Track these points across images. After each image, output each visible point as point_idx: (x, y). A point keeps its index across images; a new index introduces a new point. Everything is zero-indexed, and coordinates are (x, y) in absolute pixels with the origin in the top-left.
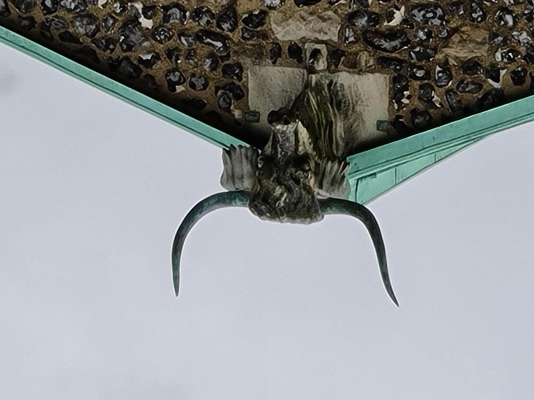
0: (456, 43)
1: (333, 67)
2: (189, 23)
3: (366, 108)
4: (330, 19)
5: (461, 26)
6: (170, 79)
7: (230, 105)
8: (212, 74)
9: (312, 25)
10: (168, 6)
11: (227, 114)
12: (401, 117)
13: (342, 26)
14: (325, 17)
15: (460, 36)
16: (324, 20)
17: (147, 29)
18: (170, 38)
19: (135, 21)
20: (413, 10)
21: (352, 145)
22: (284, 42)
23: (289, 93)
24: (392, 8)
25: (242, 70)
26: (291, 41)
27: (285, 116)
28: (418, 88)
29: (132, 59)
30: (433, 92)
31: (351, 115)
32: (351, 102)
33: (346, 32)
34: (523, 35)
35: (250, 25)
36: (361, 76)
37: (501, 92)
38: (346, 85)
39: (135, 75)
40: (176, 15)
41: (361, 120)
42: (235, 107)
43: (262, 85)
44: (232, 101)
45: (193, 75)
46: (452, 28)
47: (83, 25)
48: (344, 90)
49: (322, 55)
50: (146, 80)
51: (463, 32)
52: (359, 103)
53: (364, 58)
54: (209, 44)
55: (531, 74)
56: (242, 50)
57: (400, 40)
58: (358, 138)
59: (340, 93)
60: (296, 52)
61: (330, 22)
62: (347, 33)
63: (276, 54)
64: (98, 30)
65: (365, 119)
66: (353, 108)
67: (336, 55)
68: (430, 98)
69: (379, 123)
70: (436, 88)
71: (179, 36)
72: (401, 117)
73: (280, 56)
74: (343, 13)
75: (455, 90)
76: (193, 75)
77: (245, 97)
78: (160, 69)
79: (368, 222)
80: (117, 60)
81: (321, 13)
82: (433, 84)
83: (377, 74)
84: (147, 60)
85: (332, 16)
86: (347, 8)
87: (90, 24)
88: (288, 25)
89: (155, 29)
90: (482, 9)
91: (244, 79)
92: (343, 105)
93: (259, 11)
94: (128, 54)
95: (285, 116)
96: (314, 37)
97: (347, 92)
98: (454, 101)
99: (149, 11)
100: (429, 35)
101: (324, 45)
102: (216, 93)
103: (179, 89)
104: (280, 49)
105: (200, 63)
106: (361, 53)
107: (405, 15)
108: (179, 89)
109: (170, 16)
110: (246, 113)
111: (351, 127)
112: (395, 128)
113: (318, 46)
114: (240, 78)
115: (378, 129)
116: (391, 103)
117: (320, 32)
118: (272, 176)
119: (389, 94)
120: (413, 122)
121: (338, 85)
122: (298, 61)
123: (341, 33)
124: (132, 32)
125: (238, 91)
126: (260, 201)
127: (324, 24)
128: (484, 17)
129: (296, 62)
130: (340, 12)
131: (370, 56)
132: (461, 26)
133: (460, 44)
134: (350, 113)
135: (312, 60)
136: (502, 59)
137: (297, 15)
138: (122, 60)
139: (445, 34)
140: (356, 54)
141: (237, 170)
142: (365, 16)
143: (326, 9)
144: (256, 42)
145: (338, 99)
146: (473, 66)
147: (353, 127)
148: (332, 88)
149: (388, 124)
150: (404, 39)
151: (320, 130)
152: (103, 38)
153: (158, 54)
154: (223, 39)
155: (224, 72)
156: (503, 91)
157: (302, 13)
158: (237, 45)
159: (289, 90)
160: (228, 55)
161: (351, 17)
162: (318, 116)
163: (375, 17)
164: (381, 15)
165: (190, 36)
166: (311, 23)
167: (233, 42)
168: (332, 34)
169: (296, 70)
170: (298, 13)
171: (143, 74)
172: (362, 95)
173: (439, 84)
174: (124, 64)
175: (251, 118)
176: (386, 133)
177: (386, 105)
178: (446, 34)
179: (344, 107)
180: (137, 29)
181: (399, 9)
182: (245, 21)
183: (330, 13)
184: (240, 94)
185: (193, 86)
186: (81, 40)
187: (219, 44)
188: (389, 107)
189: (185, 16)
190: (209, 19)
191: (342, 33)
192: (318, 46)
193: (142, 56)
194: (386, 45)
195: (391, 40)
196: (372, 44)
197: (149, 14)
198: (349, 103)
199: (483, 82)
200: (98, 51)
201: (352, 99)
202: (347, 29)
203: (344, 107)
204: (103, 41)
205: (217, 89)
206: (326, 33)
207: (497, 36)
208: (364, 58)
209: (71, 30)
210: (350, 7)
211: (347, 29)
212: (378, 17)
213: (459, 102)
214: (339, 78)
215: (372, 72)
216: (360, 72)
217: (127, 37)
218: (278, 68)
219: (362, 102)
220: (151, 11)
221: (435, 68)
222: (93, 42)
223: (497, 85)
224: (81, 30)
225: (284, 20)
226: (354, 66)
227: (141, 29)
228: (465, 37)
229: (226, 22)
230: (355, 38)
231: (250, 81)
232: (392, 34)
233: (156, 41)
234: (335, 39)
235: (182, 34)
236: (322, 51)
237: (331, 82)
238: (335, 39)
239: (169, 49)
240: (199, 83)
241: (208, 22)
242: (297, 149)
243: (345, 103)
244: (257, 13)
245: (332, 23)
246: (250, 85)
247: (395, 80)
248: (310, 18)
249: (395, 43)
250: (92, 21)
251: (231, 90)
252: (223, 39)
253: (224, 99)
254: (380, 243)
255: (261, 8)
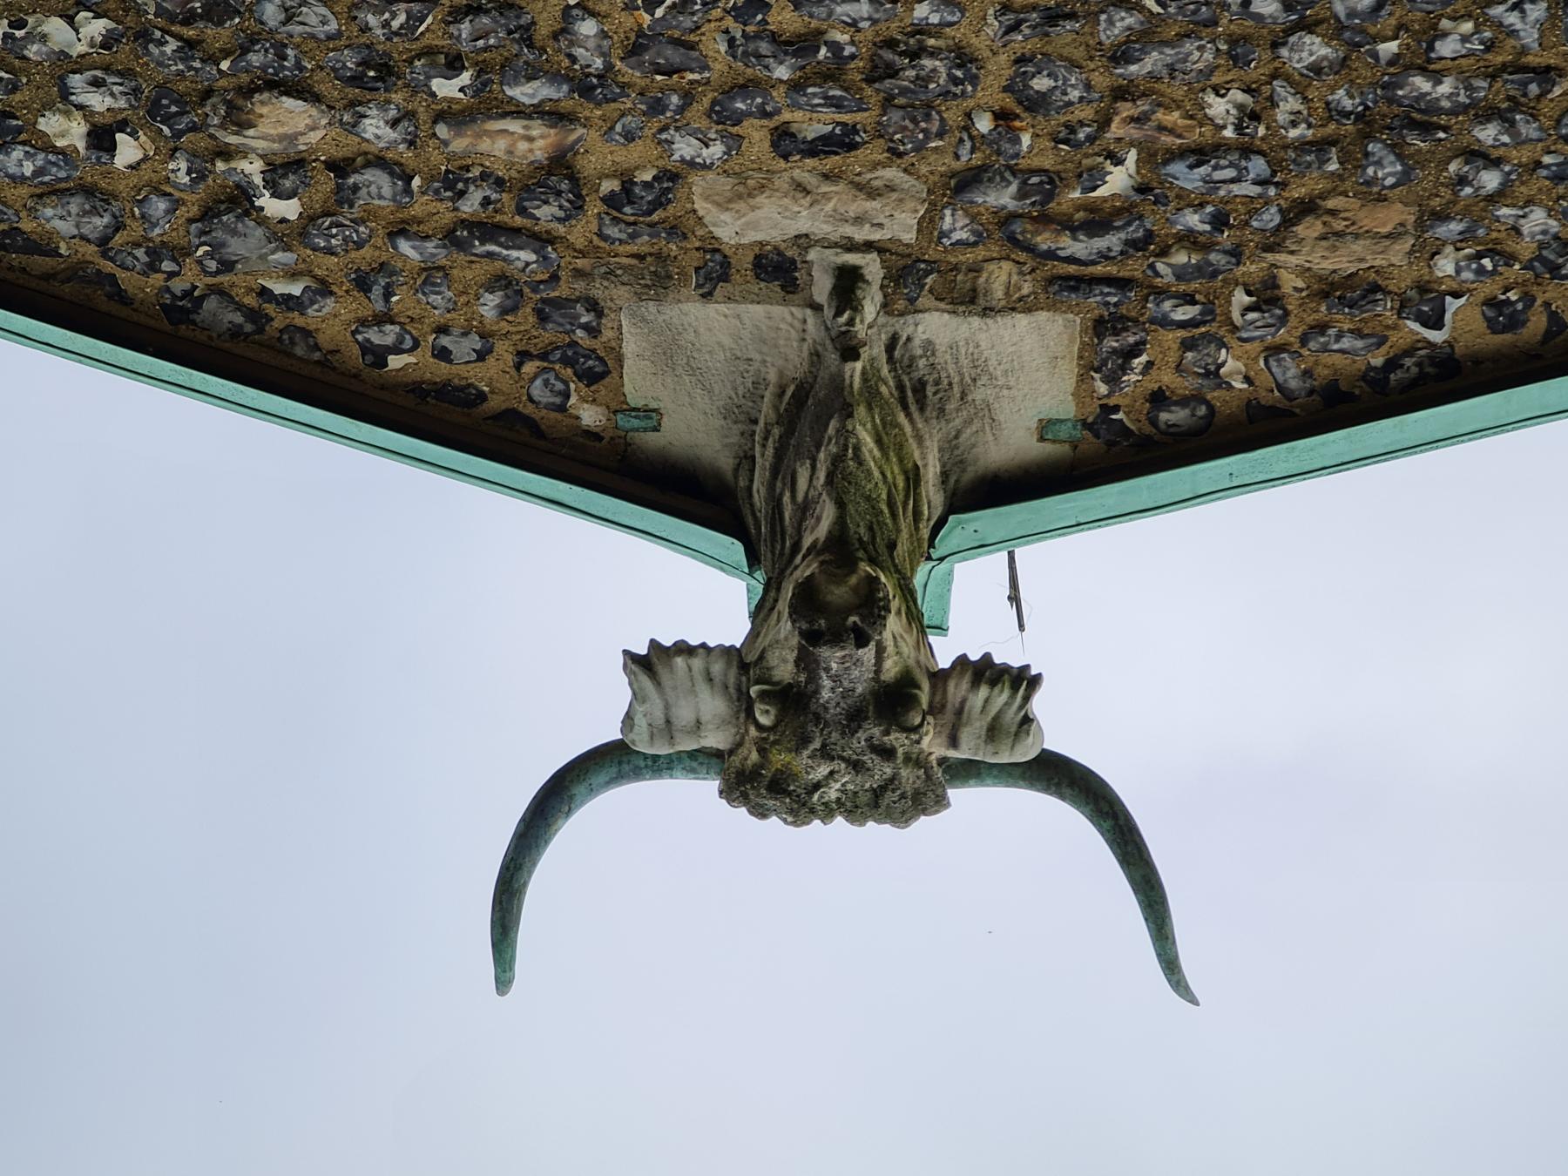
0: (1309, 242)
1: (901, 304)
2: (421, 206)
3: (1005, 392)
4: (890, 188)
5: (1323, 196)
6: (368, 340)
7: (568, 397)
8: (503, 324)
9: (830, 206)
10: (344, 160)
11: (559, 416)
12: (1116, 409)
13: (933, 204)
14: (876, 183)
15: (1324, 223)
16: (873, 194)
17: (283, 221)
18: (359, 245)
19: (240, 199)
20: (1166, 162)
21: (957, 481)
22: (738, 246)
23: (756, 365)
24: (1101, 159)
25: (600, 314)
26: (762, 244)
27: (853, 619)
28: (1175, 346)
29: (238, 292)
30: (1224, 351)
31: (958, 410)
32: (956, 380)
33: (942, 218)
34: (1532, 217)
35: (627, 210)
36: (990, 321)
37: (1448, 350)
38: (941, 342)
39: (249, 328)
40: (380, 188)
41: (987, 420)
42: (583, 400)
43: (669, 353)
44: (572, 386)
45: (442, 330)
46: (1294, 200)
47: (69, 214)
48: (933, 354)
49: (867, 282)
50: (285, 337)
51: (1333, 213)
52: (984, 380)
53: (999, 277)
54: (490, 255)
55: (1547, 305)
56: (604, 269)
57: (1123, 235)
58: (976, 460)
59: (922, 363)
60: (778, 269)
61: (894, 196)
62: (948, 219)
63: (715, 273)
64: (118, 227)
65: (1002, 418)
66: (963, 395)
67: (908, 274)
68: (1212, 368)
69: (1045, 429)
70: (1234, 343)
71: (392, 235)
72: (1116, 409)
73: (725, 277)
74: (932, 173)
75: (1296, 347)
76: (442, 330)
77: (615, 374)
78: (332, 320)
79: (1107, 825)
80: (187, 294)
81: (859, 174)
82: (1222, 332)
83: (1043, 316)
84: (290, 296)
85: (897, 181)
86: (949, 160)
87: (94, 211)
88: (753, 208)
89: (309, 219)
90: (1400, 157)
91: (608, 334)
92: (930, 390)
93: (654, 172)
94: (224, 279)
95: (853, 619)
96: (838, 235)
97: (944, 357)
98: (1290, 374)
99: (285, 176)
100: (1219, 221)
101: (874, 255)
102: (518, 366)
103: (395, 362)
104: (726, 264)
105: (463, 299)
106: (992, 266)
107: (1138, 172)
108: (395, 362)
109: (356, 188)
110: (615, 412)
111: (956, 437)
112: (1097, 436)
113: (852, 259)
114: (593, 331)
115: (1042, 439)
116: (1083, 378)
117: (858, 220)
118: (806, 748)
119: (1080, 357)
120: (1154, 422)
121: (917, 342)
122: (783, 287)
123: (928, 224)
124: (234, 233)
125: (590, 362)
126: (763, 791)
127: (876, 204)
128: (1404, 179)
129: (778, 289)
130: (924, 169)
131: (1021, 273)
132: (1323, 196)
133: (1324, 243)
134: (951, 406)
135: (846, 316)
136: (1458, 272)
137: (782, 182)
138: (203, 298)
139: (1271, 218)
140: (975, 269)
141: (684, 714)
142: (1010, 183)
143: (875, 166)
144: (645, 249)
145: (916, 375)
146: (1363, 297)
147: (964, 436)
148: (897, 354)
149: (1074, 427)
150: (1136, 231)
151: (894, 515)
152: (138, 245)
153: (322, 281)
154: (541, 240)
155: (542, 318)
156: (1452, 347)
157: (797, 173)
158: (583, 254)
159: (757, 357)
160: (555, 278)
161: (965, 182)
162: (883, 474)
163: (1042, 182)
164: (1058, 173)
165: (427, 237)
166: (829, 199)
167: (571, 246)
168: (900, 224)
169: (778, 311)
170: (786, 175)
171: (276, 324)
172: (993, 362)
173: (1245, 335)
174: (211, 304)
175: (636, 423)
176: (1066, 448)
177: (1070, 383)
178: (1277, 219)
179: (935, 394)
180: (252, 223)
181: (1119, 162)
182: (610, 200)
183: (891, 174)
184: (597, 371)
185: (443, 354)
186: (63, 250)
187: (526, 256)
188: (1078, 386)
189: (408, 191)
190: (488, 193)
191: (932, 220)
192: (852, 259)
193: (269, 284)
194: (1080, 247)
195: (1091, 236)
196: (1030, 249)
197: (287, 184)
198: (950, 384)
199: (1388, 327)
200: (121, 275)
201: (961, 374)
202: (948, 212)
203: (935, 394)
204: (140, 253)
205: (523, 356)
206: (880, 225)
207: (1442, 217)
208: (999, 277)
209: (27, 225)
210: (957, 157)
211: (948, 212)
212: (1051, 181)
213: (1307, 374)
214: (920, 329)
215: (1028, 310)
216: (988, 311)
217: (217, 247)
218: (722, 308)
219: (992, 377)
220: (292, 177)
221: (1231, 294)
222: (104, 255)
223: (1436, 336)
224: (65, 227)
225: (740, 197)
226: (968, 300)
227: (262, 221)
228: (1339, 225)
229: (546, 202)
230: (973, 232)
231: (626, 335)
232: (1097, 221)
233: (314, 250)
234: (909, 237)
235: (399, 230)
236: (865, 272)
237: (894, 339)
238: (909, 237)
239: (359, 269)
240: (463, 348)
241: (486, 202)
242: (878, 672)
243: (937, 383)
244: (647, 176)
245: (901, 200)
246: (630, 347)
247: (1101, 327)
248: (825, 188)
249: (1100, 243)
250: (98, 204)
251: (566, 361)
252: (541, 240)
253: (546, 383)
254: (1152, 888)
255: (660, 163)
